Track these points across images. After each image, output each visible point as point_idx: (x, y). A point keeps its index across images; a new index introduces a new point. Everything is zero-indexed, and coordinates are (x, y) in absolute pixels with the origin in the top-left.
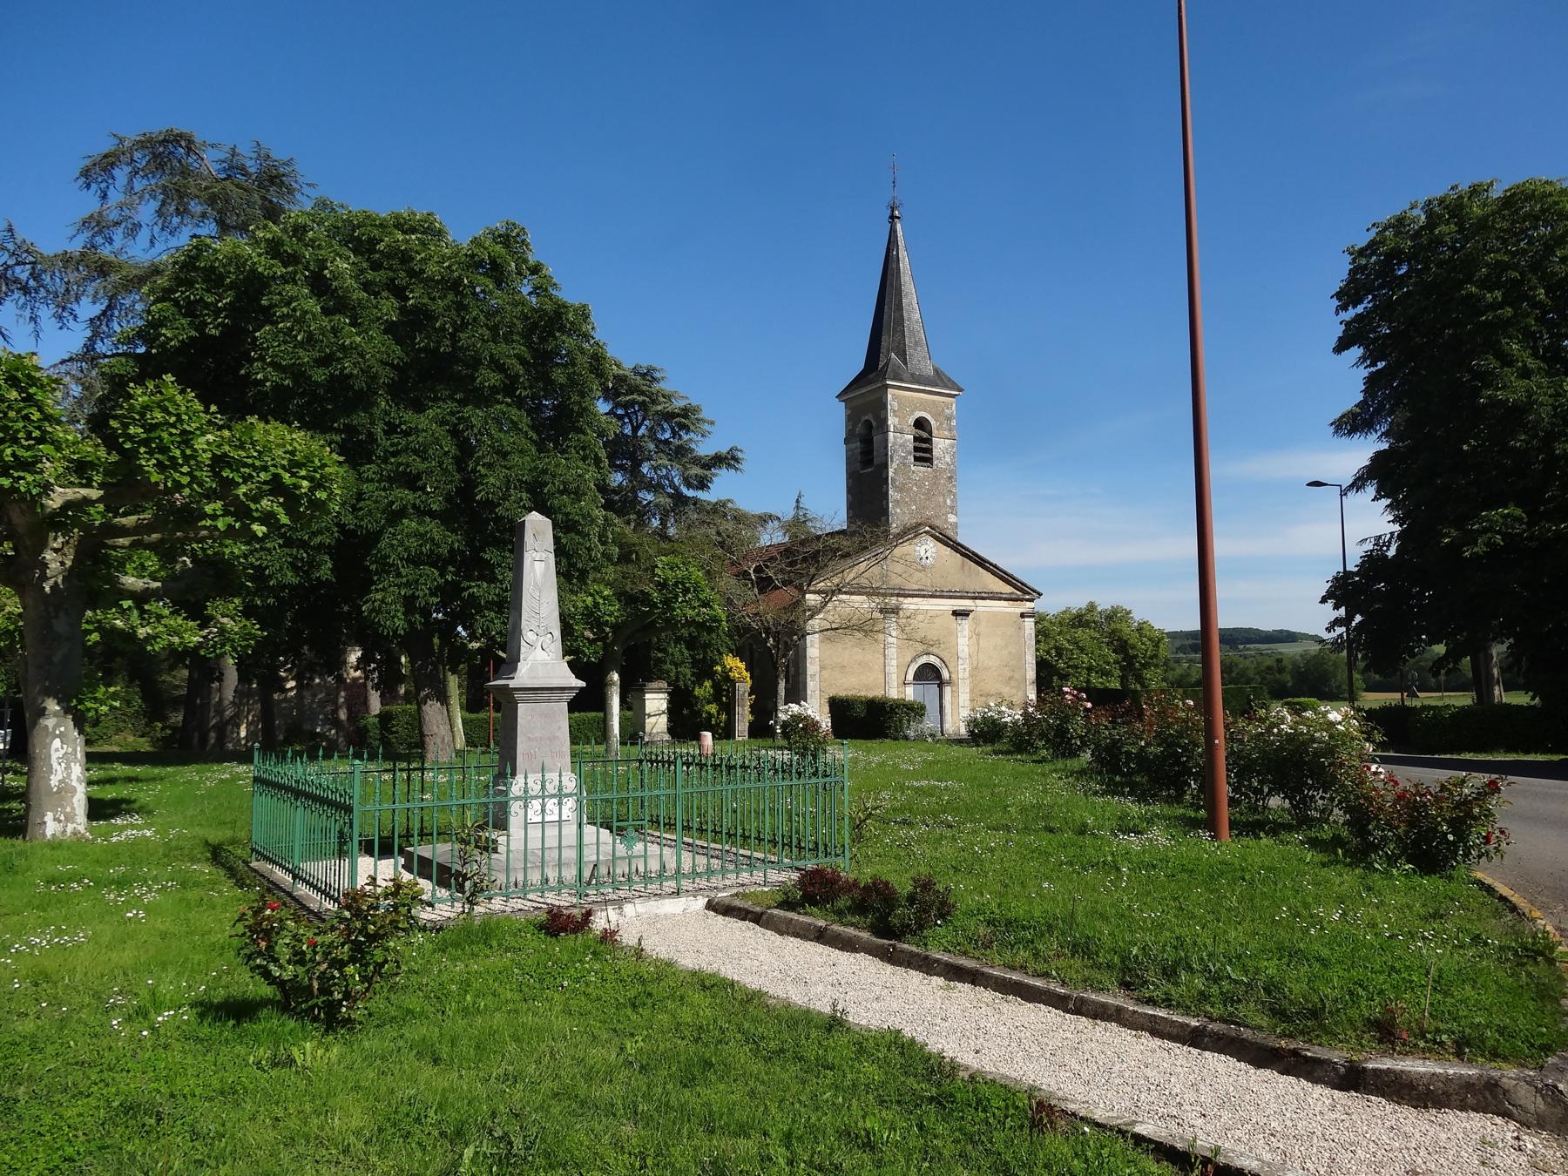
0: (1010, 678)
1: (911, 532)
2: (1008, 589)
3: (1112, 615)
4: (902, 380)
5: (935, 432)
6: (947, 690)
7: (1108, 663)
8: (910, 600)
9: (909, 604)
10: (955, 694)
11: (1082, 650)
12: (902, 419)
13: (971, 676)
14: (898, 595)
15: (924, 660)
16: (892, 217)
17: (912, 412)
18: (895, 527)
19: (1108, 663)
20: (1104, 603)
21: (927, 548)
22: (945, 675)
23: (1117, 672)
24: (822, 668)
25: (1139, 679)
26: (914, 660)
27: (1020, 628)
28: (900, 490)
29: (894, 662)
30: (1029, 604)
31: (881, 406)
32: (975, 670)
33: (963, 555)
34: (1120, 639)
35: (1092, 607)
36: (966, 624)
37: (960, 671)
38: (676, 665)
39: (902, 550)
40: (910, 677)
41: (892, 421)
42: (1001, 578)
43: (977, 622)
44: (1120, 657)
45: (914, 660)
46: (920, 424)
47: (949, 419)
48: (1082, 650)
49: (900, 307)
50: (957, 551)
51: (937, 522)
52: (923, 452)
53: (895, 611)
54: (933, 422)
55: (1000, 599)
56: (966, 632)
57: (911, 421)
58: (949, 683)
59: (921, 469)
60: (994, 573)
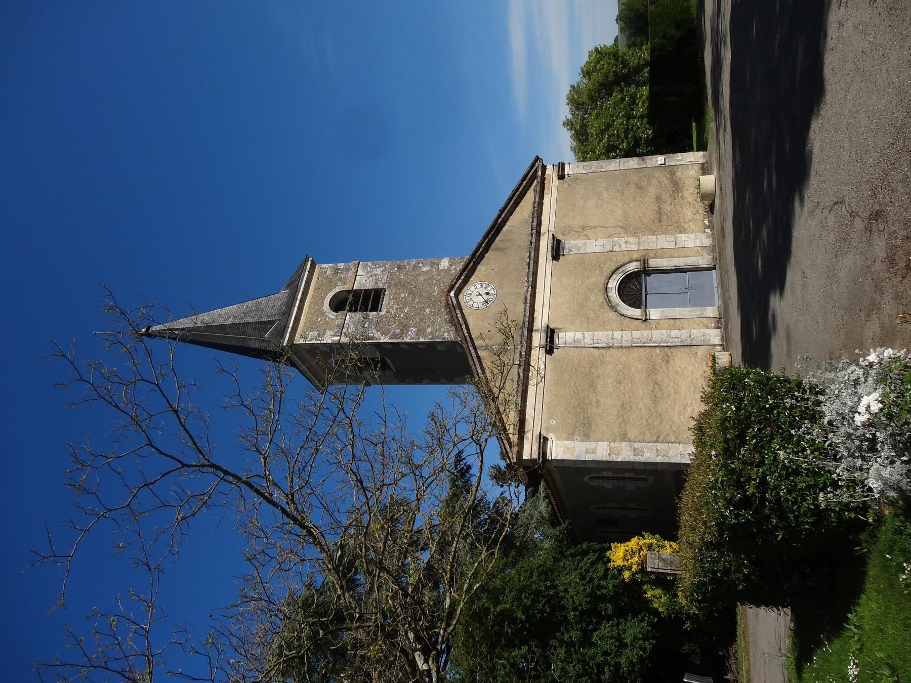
0: (638, 186)
1: (454, 311)
2: (530, 196)
3: (576, 103)
4: (285, 327)
5: (348, 287)
6: (653, 263)
7: (623, 99)
8: (537, 315)
9: (541, 320)
10: (660, 253)
11: (609, 126)
12: (328, 325)
13: (635, 234)
14: (531, 330)
15: (614, 295)
16: (148, 334)
17: (323, 314)
18: (448, 334)
19: (623, 99)
20: (565, 112)
21: (474, 296)
22: (633, 267)
23: (632, 89)
24: (624, 438)
25: (638, 70)
26: (614, 308)
27: (576, 178)
28: (405, 328)
29: (617, 335)
30: (549, 171)
31: (313, 349)
32: (627, 229)
33: (486, 250)
34: (599, 91)
35: (569, 124)
36: (571, 244)
37: (629, 247)
38: (622, 645)
39: (477, 325)
40: (636, 313)
41: (329, 338)
42: (517, 204)
43: (568, 230)
44: (617, 89)
45: (614, 308)
46: (338, 304)
47: (336, 271)
48: (609, 126)
49: (222, 328)
50: (482, 257)
51: (448, 282)
52: (368, 300)
53: (551, 333)
54: (337, 290)
55: (541, 204)
56: (580, 242)
57: (332, 315)
58: (644, 261)
59: (386, 302)
60: (511, 213)
